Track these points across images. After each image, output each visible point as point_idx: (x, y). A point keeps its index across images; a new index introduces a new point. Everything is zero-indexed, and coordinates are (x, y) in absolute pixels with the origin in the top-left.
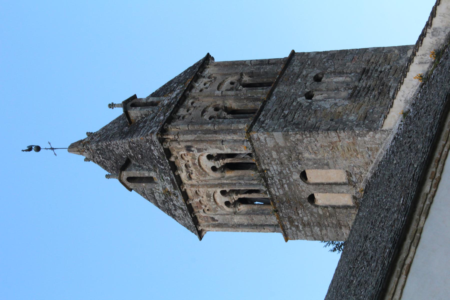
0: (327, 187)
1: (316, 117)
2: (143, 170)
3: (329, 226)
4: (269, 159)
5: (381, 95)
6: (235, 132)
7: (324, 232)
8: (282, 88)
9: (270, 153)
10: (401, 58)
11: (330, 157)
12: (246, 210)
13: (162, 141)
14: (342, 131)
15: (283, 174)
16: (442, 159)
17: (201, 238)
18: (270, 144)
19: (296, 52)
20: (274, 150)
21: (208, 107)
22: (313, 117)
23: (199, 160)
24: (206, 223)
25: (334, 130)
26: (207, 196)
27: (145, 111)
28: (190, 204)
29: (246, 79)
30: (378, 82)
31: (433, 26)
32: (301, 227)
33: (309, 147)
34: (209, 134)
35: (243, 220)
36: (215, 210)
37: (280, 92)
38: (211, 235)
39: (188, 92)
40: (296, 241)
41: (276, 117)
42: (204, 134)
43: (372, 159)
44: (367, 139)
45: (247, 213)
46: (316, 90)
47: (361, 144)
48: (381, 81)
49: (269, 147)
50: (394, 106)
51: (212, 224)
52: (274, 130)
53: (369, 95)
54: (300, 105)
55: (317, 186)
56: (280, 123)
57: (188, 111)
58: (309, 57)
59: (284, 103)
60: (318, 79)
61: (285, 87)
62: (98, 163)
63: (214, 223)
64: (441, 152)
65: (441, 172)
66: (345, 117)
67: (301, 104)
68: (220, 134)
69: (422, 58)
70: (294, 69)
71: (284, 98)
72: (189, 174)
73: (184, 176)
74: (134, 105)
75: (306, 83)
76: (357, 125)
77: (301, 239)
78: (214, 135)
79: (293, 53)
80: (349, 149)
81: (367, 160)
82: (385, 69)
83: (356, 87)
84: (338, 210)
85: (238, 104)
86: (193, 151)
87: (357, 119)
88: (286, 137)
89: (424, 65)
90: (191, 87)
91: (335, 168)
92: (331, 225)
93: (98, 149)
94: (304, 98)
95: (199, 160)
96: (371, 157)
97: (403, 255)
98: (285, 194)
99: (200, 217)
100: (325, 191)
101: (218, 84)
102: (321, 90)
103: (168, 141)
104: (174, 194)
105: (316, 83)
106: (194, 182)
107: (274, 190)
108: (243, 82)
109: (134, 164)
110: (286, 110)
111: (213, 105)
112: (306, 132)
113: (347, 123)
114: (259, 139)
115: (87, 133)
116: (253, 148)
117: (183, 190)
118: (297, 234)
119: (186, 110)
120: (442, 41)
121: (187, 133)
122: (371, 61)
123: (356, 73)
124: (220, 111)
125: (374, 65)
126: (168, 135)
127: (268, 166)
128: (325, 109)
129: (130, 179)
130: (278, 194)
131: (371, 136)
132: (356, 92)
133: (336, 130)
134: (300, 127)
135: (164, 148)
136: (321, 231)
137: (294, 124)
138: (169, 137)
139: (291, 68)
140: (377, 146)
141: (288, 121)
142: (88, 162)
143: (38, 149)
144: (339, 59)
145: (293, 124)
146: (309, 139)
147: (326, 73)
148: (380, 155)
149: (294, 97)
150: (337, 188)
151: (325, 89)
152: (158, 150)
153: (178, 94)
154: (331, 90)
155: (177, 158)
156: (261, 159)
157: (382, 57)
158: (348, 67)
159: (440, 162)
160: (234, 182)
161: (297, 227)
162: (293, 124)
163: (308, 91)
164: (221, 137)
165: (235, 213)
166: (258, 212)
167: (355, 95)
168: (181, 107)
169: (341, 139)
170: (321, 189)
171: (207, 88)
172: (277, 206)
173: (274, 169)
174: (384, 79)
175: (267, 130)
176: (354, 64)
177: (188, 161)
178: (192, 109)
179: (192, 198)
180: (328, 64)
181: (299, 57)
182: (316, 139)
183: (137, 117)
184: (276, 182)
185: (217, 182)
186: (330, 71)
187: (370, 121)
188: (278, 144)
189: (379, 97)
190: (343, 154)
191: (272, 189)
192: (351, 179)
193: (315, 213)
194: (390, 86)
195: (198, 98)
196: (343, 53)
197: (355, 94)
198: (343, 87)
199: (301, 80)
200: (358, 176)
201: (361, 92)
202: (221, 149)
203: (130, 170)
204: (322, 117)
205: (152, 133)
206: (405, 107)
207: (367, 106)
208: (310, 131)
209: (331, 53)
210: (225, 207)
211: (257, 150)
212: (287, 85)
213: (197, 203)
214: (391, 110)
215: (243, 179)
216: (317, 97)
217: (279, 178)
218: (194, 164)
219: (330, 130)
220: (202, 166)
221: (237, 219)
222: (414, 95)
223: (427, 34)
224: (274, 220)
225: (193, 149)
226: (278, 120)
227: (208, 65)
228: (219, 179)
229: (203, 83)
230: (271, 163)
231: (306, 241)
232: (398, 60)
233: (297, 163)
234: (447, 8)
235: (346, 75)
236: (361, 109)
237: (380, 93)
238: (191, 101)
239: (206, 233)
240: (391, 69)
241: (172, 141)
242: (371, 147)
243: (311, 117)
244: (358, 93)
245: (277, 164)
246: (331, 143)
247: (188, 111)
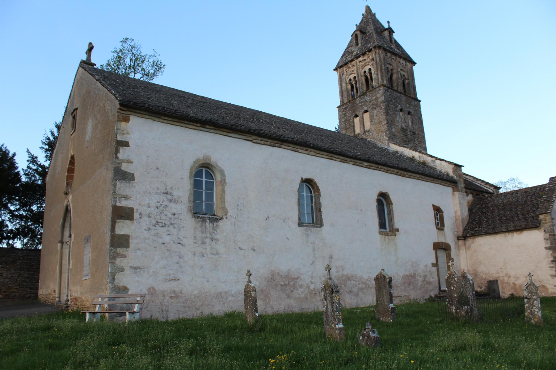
6: (382, 79)
8: (404, 98)
13: (375, 47)
17: (334, 70)
18: (378, 95)
27: (388, 38)
29: (406, 81)
36: (347, 75)
38: (336, 74)
44: (385, 137)
45: (347, 89)
52: (385, 96)
54: (397, 107)
60: (409, 113)
62: (362, 20)
73: (361, 59)
79: (420, 101)
88: (382, 102)
90: (400, 57)
97: (336, 156)
98: (357, 104)
106: (358, 64)
128: (396, 118)
129: (356, 35)
148: (379, 143)
150: (362, 127)
161: (344, 111)
164: (379, 73)
165: (347, 84)
167: (402, 129)
173: (368, 98)
216: (401, 114)
221: (344, 85)
224: (346, 101)
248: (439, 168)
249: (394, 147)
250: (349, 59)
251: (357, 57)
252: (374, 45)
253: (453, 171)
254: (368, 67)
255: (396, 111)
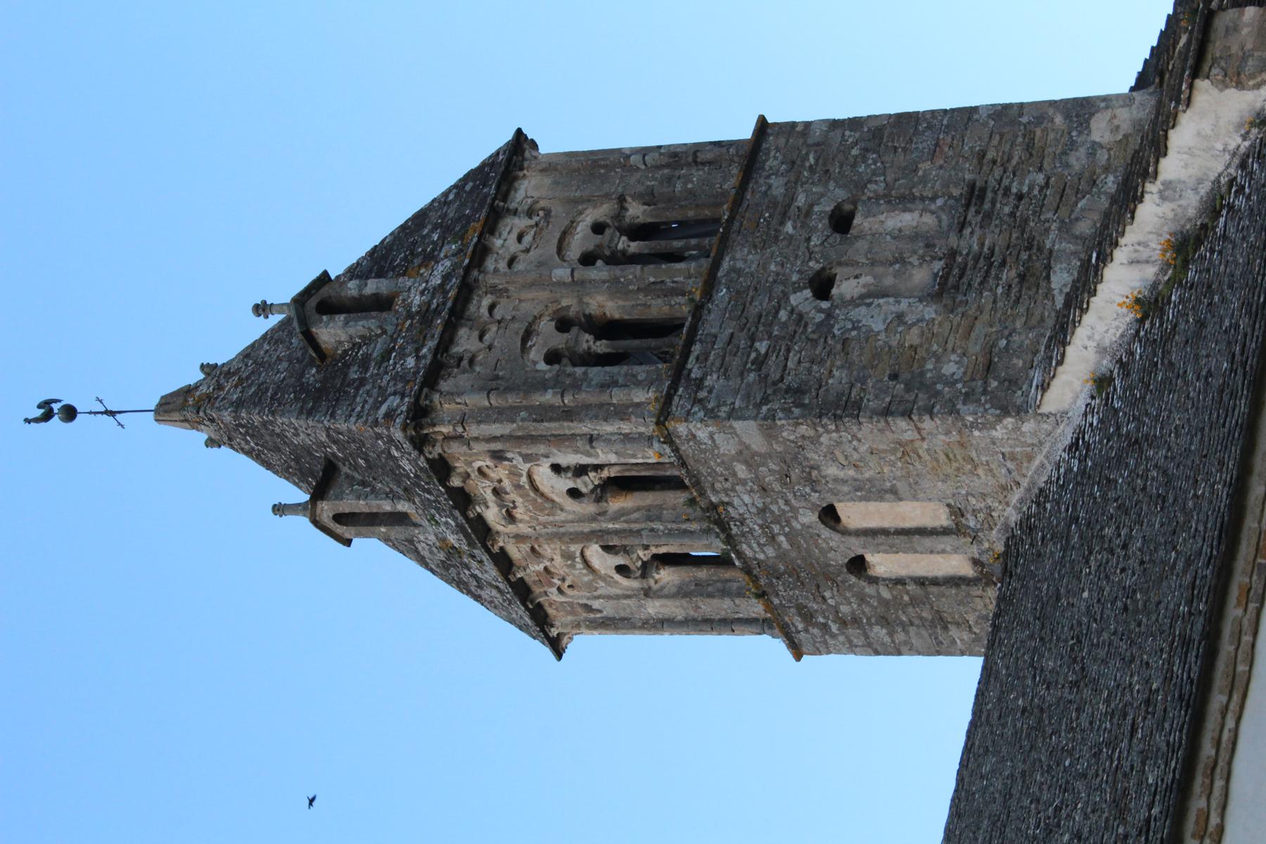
0: (897, 540)
1: (848, 365)
2: (376, 498)
3: (912, 624)
4: (726, 480)
5: (1026, 285)
6: (621, 413)
7: (900, 637)
8: (742, 258)
9: (729, 468)
10: (1072, 145)
11: (899, 473)
12: (676, 582)
13: (420, 443)
14: (926, 417)
15: (772, 512)
16: (1224, 755)
17: (559, 654)
18: (727, 446)
19: (770, 120)
20: (738, 461)
21: (537, 318)
22: (838, 363)
23: (530, 476)
24: (570, 618)
25: (903, 414)
26: (562, 556)
27: (362, 326)
28: (522, 579)
29: (636, 211)
30: (1014, 235)
31: (1161, 178)
32: (834, 628)
33: (837, 452)
34: (551, 420)
35: (675, 609)
36: (590, 587)
37: (739, 272)
38: (586, 646)
39: (475, 273)
40: (824, 657)
41: (736, 362)
42: (535, 420)
43: (1018, 479)
44: (998, 433)
45: (682, 593)
46: (840, 264)
47: (983, 445)
48: (1023, 232)
49: (724, 455)
50: (1068, 359)
51: (586, 620)
52: (733, 414)
53: (991, 281)
55: (870, 539)
56: (749, 385)
57: (481, 338)
58: (810, 141)
59: (753, 310)
60: (841, 222)
61: (749, 253)
62: (248, 453)
63: (592, 616)
64: (1216, 735)
65: (1224, 807)
66: (930, 366)
67: (801, 316)
68: (581, 421)
69: (1136, 251)
70: (770, 187)
71: (751, 293)
72: (507, 511)
73: (492, 515)
74: (329, 308)
75: (808, 240)
76: (967, 394)
77: (839, 652)
78: (566, 424)
79: (763, 126)
80: (951, 456)
81: (1003, 481)
82: (1031, 188)
83: (953, 254)
84: (934, 589)
85: (621, 303)
86: (510, 460)
87: (965, 373)
88: (770, 432)
89: (1145, 266)
91: (915, 498)
92: (917, 622)
93: (240, 425)
94: (808, 293)
95: (530, 476)
96: (1015, 474)
98: (782, 556)
99: (550, 605)
100: (894, 549)
101: (558, 235)
102: (854, 264)
103: (436, 441)
104: (473, 557)
105: (838, 236)
106: (523, 528)
107: (750, 547)
108: (627, 220)
109: (347, 476)
110: (761, 340)
111: (550, 310)
112: (825, 421)
113: (939, 387)
114: (694, 436)
115: (202, 367)
116: (680, 458)
117: (496, 549)
118: (825, 642)
119: (476, 334)
120: (1191, 212)
121: (488, 416)
122: (991, 155)
123: (950, 196)
124: (575, 330)
125: (997, 172)
126: (434, 425)
127: (727, 495)
128: (870, 335)
129: (339, 518)
130: (762, 557)
131: (1010, 427)
132: (956, 271)
133: (907, 414)
134: (807, 401)
135: (427, 460)
136: (891, 634)
137: (788, 390)
138: (436, 429)
139: (761, 181)
140: (1029, 449)
141: (769, 381)
142: (216, 449)
143: (70, 413)
144: (895, 149)
145: (787, 392)
146: (834, 435)
147: (864, 198)
149: (779, 289)
150: (928, 542)
151: (864, 261)
152: (413, 462)
153: (446, 277)
154: (882, 263)
155: (468, 476)
156: (706, 482)
157: (1020, 139)
158: (924, 180)
159: (1218, 770)
160: (635, 526)
161: (825, 627)
162: (787, 392)
163: (817, 267)
164: (585, 428)
165: (647, 593)
166: (710, 589)
167: (946, 289)
168: (462, 326)
169: (925, 435)
170: (882, 544)
171: (527, 251)
172: (762, 582)
173: (743, 502)
174: (1032, 224)
175: (712, 414)
176: (941, 167)
177: (500, 481)
178: (494, 328)
179: (524, 564)
180: (868, 166)
181: (782, 141)
182: (854, 437)
183: (340, 342)
184: (751, 531)
185: (587, 528)
186: (875, 192)
187: (1001, 383)
188: (748, 447)
189: (1020, 291)
190: (933, 468)
191: (744, 546)
192: (964, 521)
193: (871, 597)
194: (1051, 252)
195: (507, 290)
196: (906, 124)
197: (951, 280)
198: (915, 252)
199: (795, 228)
200: (981, 516)
201: (968, 272)
202: (588, 455)
203: (339, 497)
204: (864, 367)
205: (390, 416)
206: (1099, 363)
207: (991, 326)
208: (835, 415)
209: (872, 124)
210: (617, 577)
211: (691, 462)
212: (755, 247)
213: (538, 573)
214: (1060, 369)
215: (659, 518)
216: (846, 288)
217: (760, 522)
218: (518, 487)
219: (892, 414)
220: (541, 487)
221: (653, 608)
222: (1122, 336)
223: (1147, 197)
224: (756, 608)
225: (509, 455)
226: (742, 374)
227: (521, 169)
228: (593, 519)
229: (514, 236)
230: (733, 490)
231: (852, 657)
232: (1064, 153)
233: (808, 490)
234: (1199, 134)
235: (921, 207)
236: (973, 335)
237: (1022, 277)
238: (486, 302)
239: (571, 639)
240: (1047, 184)
241: (448, 438)
242: (1012, 453)
243: (832, 365)
244: (960, 278)
245: (752, 491)
246: (900, 443)
247: (481, 338)
248: (1217, 166)
249: (1069, 388)
250: (491, 572)
251: (481, 532)
252: (407, 446)
253: (1240, 85)
254: (543, 474)
255: (825, 326)
